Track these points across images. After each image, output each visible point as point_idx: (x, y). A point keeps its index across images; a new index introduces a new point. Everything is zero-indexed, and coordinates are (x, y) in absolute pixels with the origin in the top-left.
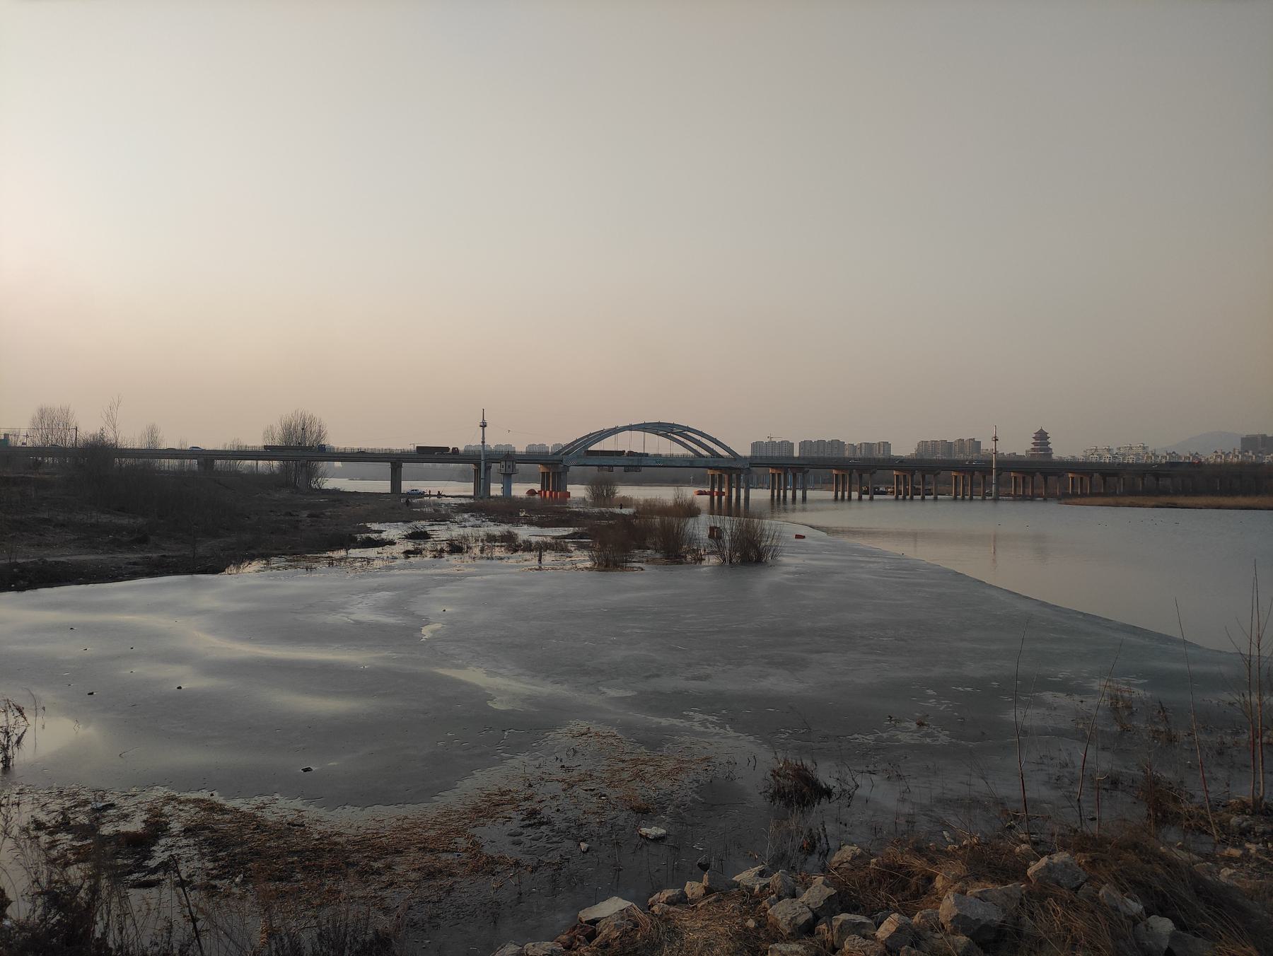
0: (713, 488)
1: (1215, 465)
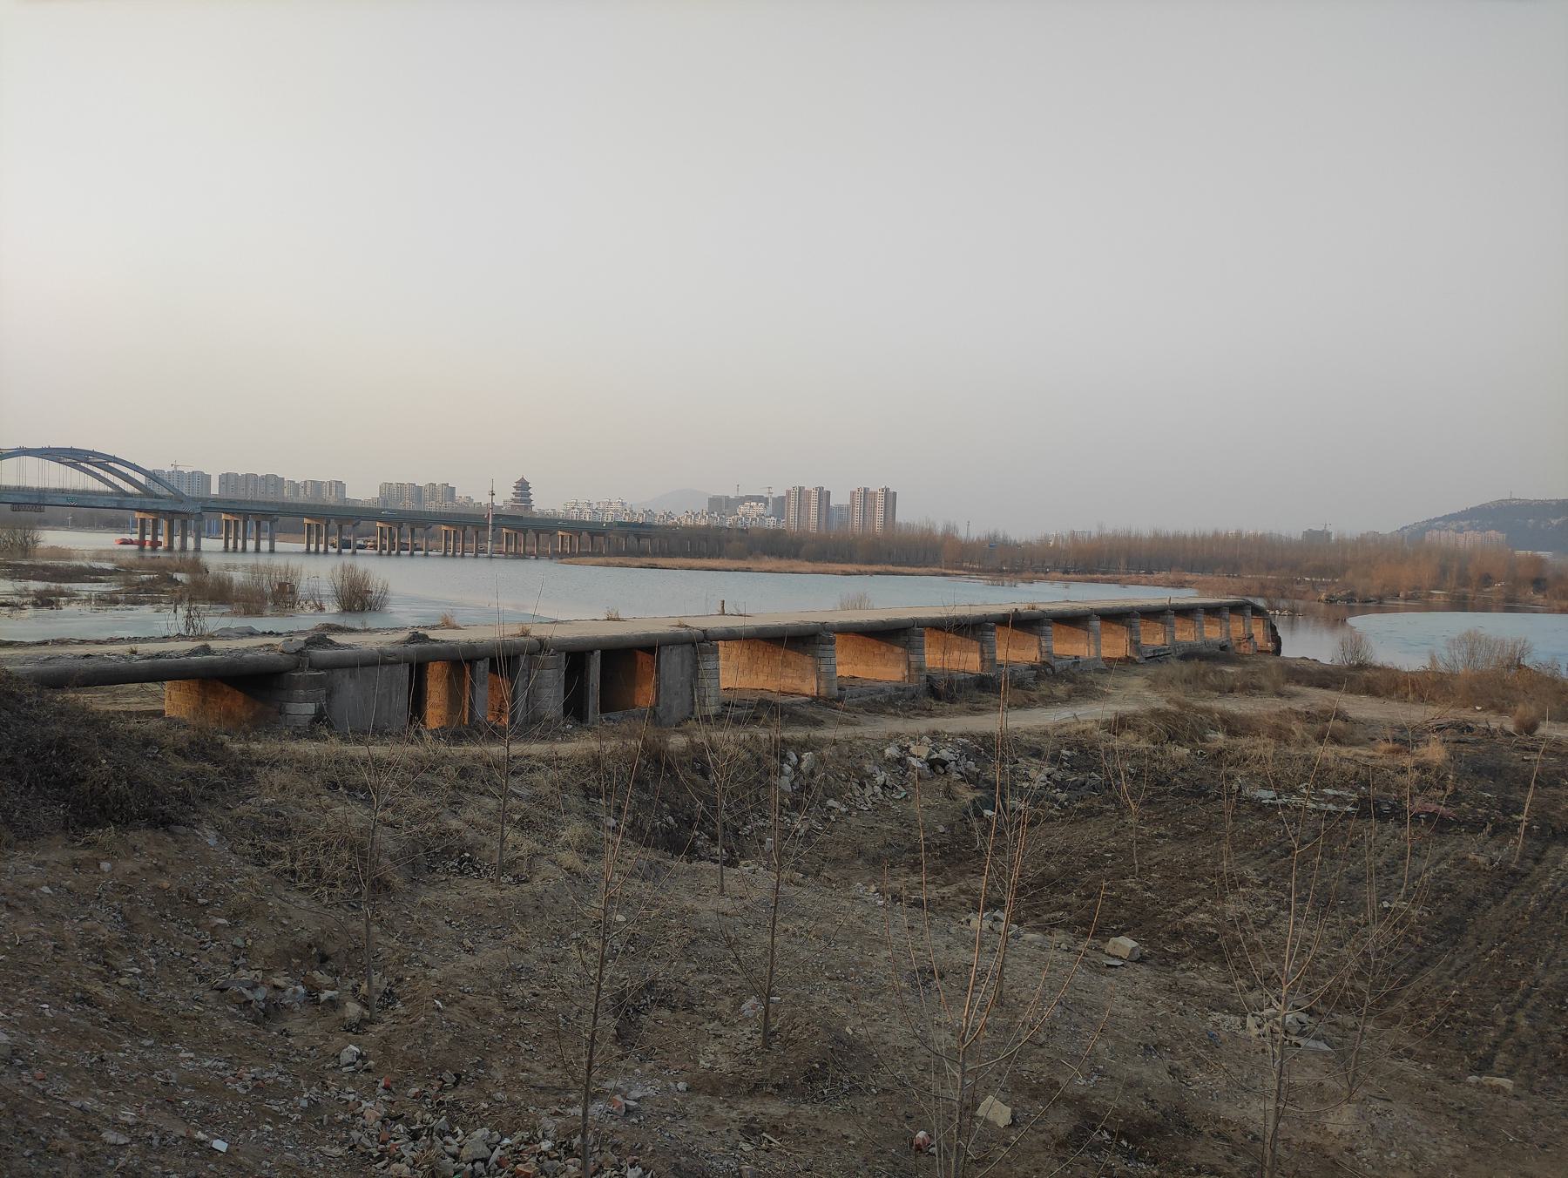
0: (143, 534)
1: (686, 528)
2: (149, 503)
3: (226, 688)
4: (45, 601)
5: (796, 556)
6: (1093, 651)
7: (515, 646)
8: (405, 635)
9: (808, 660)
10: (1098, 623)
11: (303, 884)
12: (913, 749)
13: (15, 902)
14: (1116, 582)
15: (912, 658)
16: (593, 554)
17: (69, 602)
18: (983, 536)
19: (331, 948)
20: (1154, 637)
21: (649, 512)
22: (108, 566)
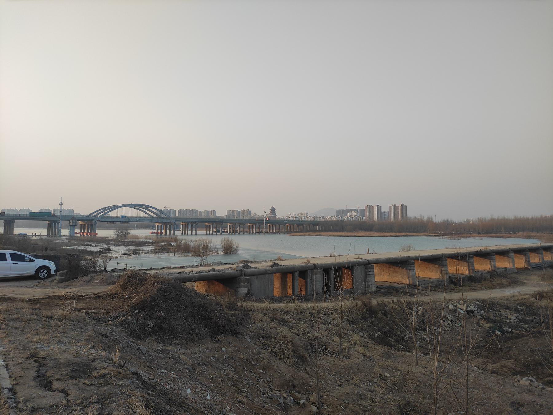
1: (330, 221)
2: (160, 220)
3: (216, 283)
4: (136, 253)
5: (371, 230)
6: (511, 265)
7: (306, 267)
8: (271, 263)
9: (404, 270)
10: (513, 254)
11: (279, 357)
12: (459, 306)
13: (206, 363)
14: (501, 237)
15: (443, 269)
16: (298, 232)
17: (142, 253)
18: (442, 221)
19: (296, 383)
20: (535, 259)
21: (315, 216)
22: (150, 241)
